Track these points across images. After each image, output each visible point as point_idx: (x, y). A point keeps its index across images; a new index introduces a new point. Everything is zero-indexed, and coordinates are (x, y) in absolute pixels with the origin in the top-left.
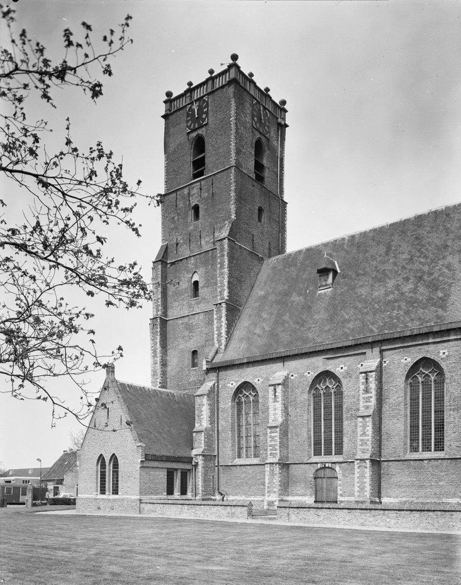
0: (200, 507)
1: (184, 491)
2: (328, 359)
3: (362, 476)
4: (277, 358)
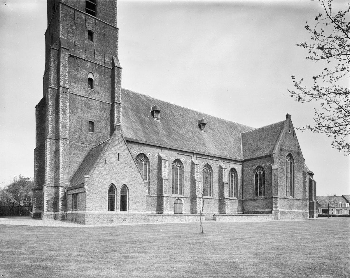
0: (183, 217)
2: (178, 154)
4: (159, 147)
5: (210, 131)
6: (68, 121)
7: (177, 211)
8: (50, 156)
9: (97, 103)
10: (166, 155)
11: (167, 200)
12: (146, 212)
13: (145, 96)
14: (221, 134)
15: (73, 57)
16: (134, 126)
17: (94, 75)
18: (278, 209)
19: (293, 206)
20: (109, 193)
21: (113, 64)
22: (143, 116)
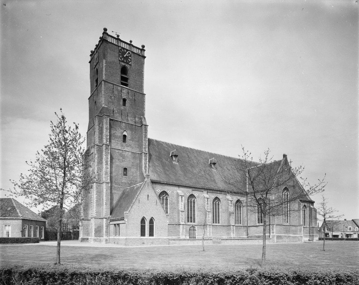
1: (151, 234)
3: (210, 230)
5: (219, 168)
6: (109, 169)
7: (192, 236)
8: (96, 195)
9: (130, 154)
10: (183, 191)
11: (183, 227)
12: (168, 237)
13: (166, 143)
14: (229, 170)
15: (112, 120)
16: (157, 169)
17: (128, 132)
18: (274, 234)
19: (289, 231)
20: (141, 224)
21: (141, 122)
22: (164, 160)
